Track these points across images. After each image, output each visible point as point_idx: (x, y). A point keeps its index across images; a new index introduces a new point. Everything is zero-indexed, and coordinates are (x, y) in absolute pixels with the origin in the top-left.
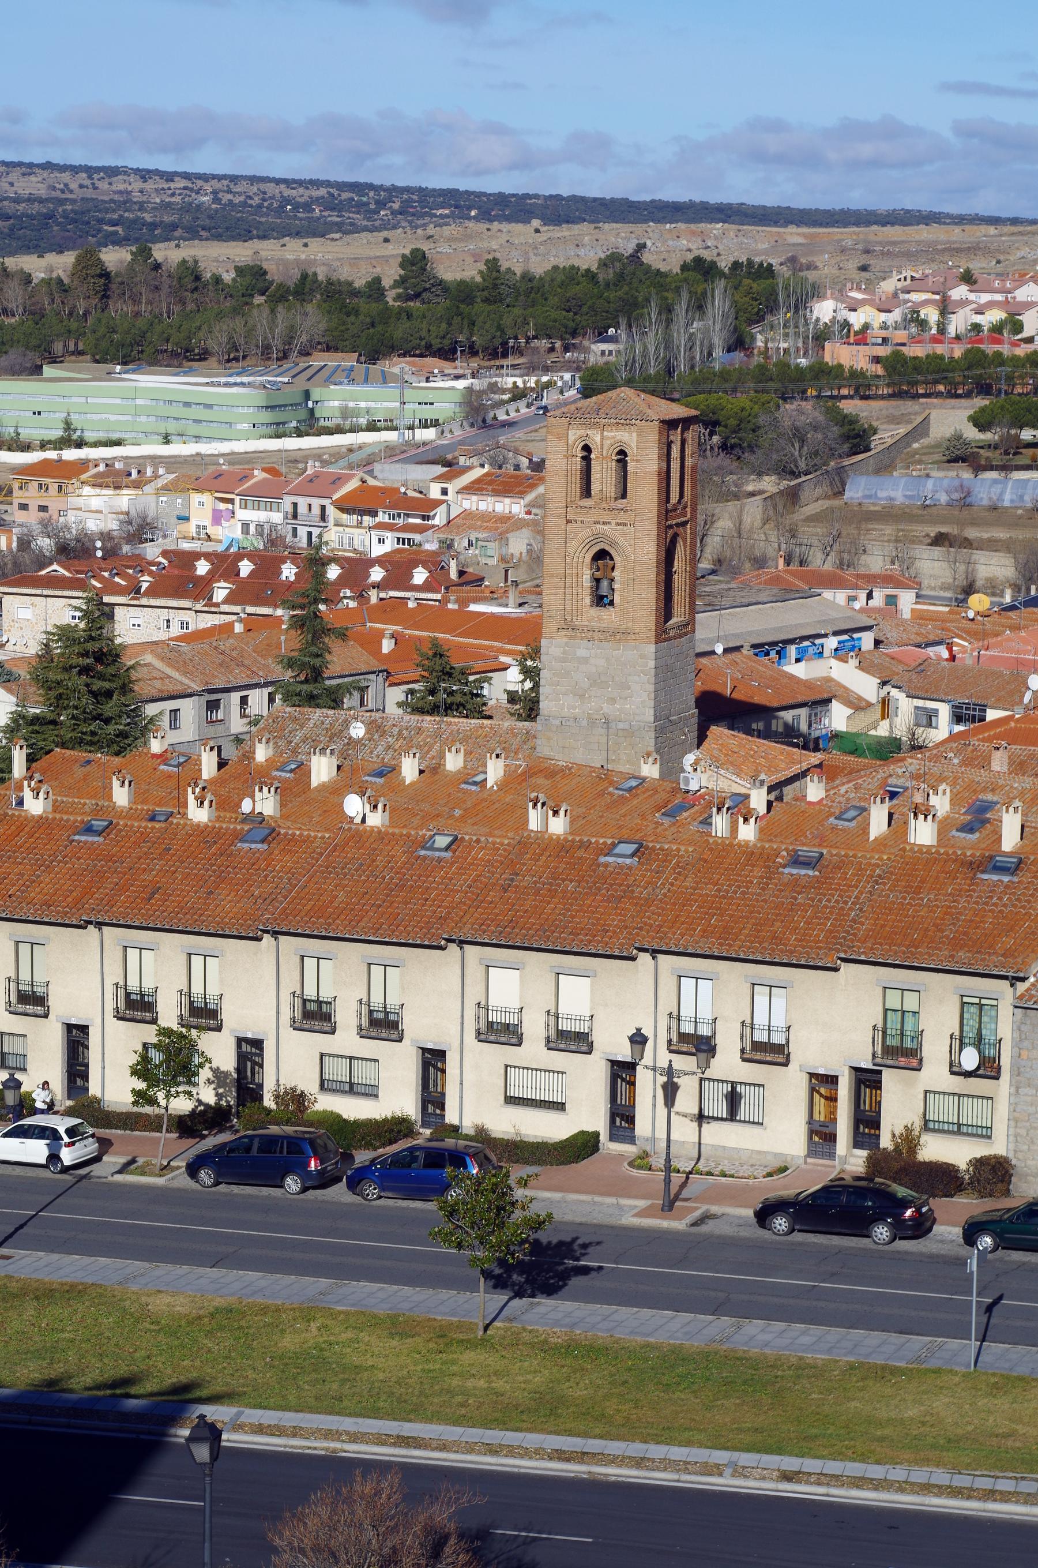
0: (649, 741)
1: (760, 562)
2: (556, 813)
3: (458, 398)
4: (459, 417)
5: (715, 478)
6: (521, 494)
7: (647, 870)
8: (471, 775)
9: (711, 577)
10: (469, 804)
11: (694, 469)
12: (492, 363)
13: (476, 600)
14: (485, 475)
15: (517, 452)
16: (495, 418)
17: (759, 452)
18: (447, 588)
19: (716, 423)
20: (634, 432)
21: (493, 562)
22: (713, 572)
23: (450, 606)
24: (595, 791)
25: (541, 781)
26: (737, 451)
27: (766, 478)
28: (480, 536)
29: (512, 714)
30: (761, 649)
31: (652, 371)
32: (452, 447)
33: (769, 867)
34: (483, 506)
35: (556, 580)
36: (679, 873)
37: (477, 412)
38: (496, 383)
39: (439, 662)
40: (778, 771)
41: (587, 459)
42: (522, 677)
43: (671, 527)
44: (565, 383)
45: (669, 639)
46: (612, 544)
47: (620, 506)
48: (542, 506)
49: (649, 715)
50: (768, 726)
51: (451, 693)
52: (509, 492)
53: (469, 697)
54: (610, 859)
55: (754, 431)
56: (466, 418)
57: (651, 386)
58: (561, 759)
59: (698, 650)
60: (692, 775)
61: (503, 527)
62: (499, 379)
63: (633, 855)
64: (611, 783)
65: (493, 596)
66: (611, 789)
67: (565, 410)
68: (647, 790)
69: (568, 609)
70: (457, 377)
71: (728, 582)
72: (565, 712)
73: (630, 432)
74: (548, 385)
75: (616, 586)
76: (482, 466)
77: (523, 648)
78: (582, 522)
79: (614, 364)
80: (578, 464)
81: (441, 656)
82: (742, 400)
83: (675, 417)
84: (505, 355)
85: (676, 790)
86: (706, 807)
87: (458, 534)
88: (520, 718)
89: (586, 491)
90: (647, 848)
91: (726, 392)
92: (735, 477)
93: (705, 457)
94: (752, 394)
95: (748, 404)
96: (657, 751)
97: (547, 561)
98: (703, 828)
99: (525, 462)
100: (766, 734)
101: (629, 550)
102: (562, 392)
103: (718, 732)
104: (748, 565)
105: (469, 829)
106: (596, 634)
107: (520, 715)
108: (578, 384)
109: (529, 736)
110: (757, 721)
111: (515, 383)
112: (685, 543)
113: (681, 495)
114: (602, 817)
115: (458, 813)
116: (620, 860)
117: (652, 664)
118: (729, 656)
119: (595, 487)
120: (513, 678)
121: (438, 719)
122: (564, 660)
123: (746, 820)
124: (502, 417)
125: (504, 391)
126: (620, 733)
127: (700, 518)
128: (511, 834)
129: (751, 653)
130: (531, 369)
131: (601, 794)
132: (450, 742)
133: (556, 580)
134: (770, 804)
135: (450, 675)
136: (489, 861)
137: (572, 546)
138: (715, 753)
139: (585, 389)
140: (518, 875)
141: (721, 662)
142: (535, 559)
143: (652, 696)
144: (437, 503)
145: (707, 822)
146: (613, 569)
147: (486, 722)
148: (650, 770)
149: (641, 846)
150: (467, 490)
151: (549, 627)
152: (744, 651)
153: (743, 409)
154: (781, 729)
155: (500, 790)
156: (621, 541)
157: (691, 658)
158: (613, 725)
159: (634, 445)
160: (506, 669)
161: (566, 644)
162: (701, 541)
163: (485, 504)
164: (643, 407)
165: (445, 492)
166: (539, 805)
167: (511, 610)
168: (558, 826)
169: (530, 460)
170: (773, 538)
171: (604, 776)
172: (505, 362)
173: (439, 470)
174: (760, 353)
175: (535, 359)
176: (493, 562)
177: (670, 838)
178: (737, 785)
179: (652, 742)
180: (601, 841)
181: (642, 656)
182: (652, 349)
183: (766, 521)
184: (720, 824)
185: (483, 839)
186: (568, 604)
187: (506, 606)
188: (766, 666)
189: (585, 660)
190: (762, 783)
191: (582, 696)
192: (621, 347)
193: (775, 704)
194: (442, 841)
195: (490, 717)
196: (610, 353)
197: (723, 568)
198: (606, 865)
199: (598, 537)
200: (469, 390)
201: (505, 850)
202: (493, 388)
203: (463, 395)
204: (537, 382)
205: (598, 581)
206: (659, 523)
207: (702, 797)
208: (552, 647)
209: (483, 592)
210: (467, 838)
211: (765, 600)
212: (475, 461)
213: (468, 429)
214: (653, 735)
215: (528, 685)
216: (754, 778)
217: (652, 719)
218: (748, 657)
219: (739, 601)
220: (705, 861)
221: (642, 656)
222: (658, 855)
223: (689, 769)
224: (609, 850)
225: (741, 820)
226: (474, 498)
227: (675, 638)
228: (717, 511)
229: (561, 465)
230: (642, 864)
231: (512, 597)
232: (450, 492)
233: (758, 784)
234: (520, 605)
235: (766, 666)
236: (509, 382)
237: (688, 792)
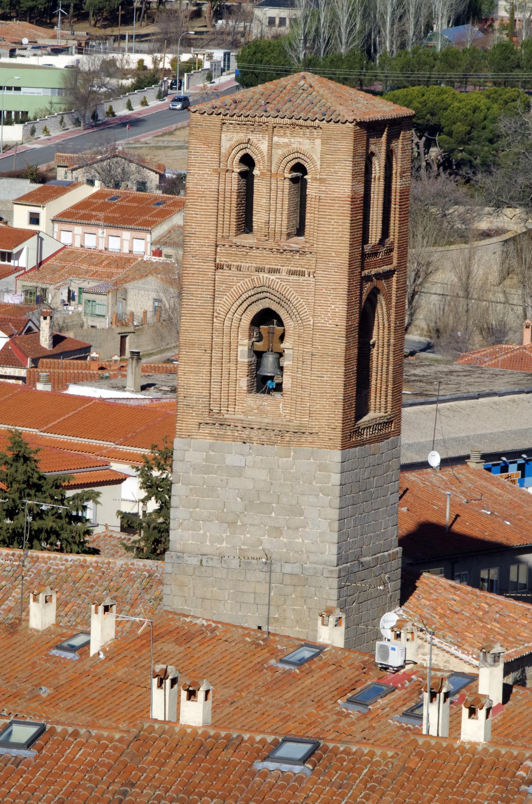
0: (329, 592)
1: (496, 334)
2: (192, 695)
3: (56, 81)
4: (59, 109)
5: (433, 210)
6: (147, 226)
7: (324, 783)
8: (67, 638)
9: (423, 355)
10: (62, 679)
11: (405, 194)
12: (108, 31)
13: (78, 380)
14: (96, 196)
15: (142, 163)
16: (111, 113)
17: (498, 173)
18: (35, 361)
19: (436, 129)
20: (318, 137)
21: (103, 324)
22: (428, 347)
23: (40, 387)
24: (252, 664)
25: (168, 647)
26: (465, 170)
27: (508, 211)
28: (86, 285)
29: (128, 549)
30: (495, 461)
31: (343, 50)
32: (46, 154)
33: (506, 784)
34: (90, 242)
35: (197, 352)
36: (373, 789)
37: (85, 105)
38: (113, 62)
39: (22, 468)
40: (518, 642)
41: (247, 176)
42: (143, 494)
43: (368, 278)
44: (215, 64)
45: (362, 444)
46: (282, 301)
47: (295, 246)
48: (181, 245)
49: (331, 553)
50: (504, 574)
51: (39, 515)
52: (131, 222)
53: (66, 520)
54: (270, 765)
55: (491, 141)
56: (68, 111)
57: (341, 72)
58: (200, 616)
59: (404, 460)
60: (394, 644)
61: (120, 273)
62: (118, 56)
63: (304, 760)
64: (273, 653)
65: (102, 374)
66: (273, 662)
67: (217, 102)
68: (326, 664)
69: (215, 395)
70: (56, 51)
71: (448, 363)
72: (208, 547)
73: (312, 139)
74: (191, 67)
75: (286, 363)
76: (91, 182)
77: (146, 452)
78: (239, 268)
79: (287, 38)
80: (233, 182)
81: (26, 459)
82: (475, 96)
83: (379, 117)
84: (127, 21)
85: (368, 666)
86: (412, 692)
87: (53, 281)
88: (140, 554)
89: (246, 224)
90: (326, 750)
91: (451, 83)
92: (461, 209)
93: (418, 178)
94: (490, 87)
95: (483, 102)
96: (342, 607)
97: (185, 323)
98: (409, 723)
99: (153, 179)
100: (501, 587)
101: (306, 311)
102: (210, 78)
103: (430, 581)
104: (477, 338)
105: (62, 716)
106: (254, 434)
107: (140, 550)
108: (234, 65)
109: (153, 581)
110: (489, 567)
111: (141, 62)
112: (388, 303)
113: (385, 232)
114: (258, 702)
115: (45, 692)
116: (285, 767)
117: (336, 478)
118: (450, 470)
119: (259, 218)
120: (131, 495)
121: (19, 552)
122: (207, 470)
123: (472, 712)
124: (122, 111)
125: (124, 74)
126: (287, 580)
127: (411, 267)
128: (123, 726)
129: (481, 466)
130: (165, 42)
131: (259, 668)
132: (35, 588)
133: (197, 352)
134: (507, 691)
135: (38, 488)
136: (91, 764)
137: (224, 302)
138: (426, 612)
139: (244, 74)
140: (133, 785)
141: (435, 478)
142: (167, 322)
143: (336, 525)
144: (22, 236)
145: (414, 713)
146: (282, 338)
147: (90, 559)
148: (331, 635)
149: (317, 746)
150: (67, 217)
151: (186, 422)
152: (472, 464)
153: (475, 109)
154: (523, 580)
155: (109, 658)
156: (294, 297)
157: (394, 472)
158: (276, 567)
159: (317, 157)
160: (119, 481)
161: (211, 447)
162: (410, 302)
163: (75, 236)
164: (331, 102)
165: (34, 219)
166: (168, 682)
167: (129, 395)
168: (194, 714)
169: (162, 177)
170: (515, 299)
171: (263, 641)
172: (127, 31)
173: (27, 186)
174: (503, 27)
175: (172, 27)
176: (103, 324)
177: (359, 737)
178: (460, 661)
179: (334, 594)
180: (258, 738)
181: (324, 465)
182: (344, 19)
183: (506, 273)
184: (433, 716)
185: (83, 731)
186: (215, 387)
187: (123, 388)
188: (503, 487)
189: (239, 471)
190: (496, 657)
191: (232, 524)
192: (298, 13)
193: (516, 542)
194: (22, 733)
195: (95, 552)
196: (282, 21)
197: (443, 341)
198: (265, 774)
199: (261, 291)
200: (74, 70)
201: (115, 748)
202: (110, 68)
203: (65, 79)
204: (174, 62)
205: (259, 355)
206: (351, 273)
207: (408, 676)
208: (190, 452)
209: (88, 367)
210: (59, 729)
211: (503, 389)
212: (80, 175)
213: (71, 127)
214: (335, 583)
215: (153, 505)
216: (485, 650)
217: (334, 558)
218: (475, 473)
219: (464, 390)
220: (412, 771)
221: (322, 467)
222: (342, 760)
223: (388, 634)
224: (269, 752)
225: (465, 712)
226: (78, 229)
227: (370, 441)
228: (435, 257)
229: (209, 183)
230: (319, 775)
231: (132, 377)
232: (43, 219)
233: (490, 659)
234: (144, 388)
235: (503, 487)
236: (133, 60)
237: (386, 668)
